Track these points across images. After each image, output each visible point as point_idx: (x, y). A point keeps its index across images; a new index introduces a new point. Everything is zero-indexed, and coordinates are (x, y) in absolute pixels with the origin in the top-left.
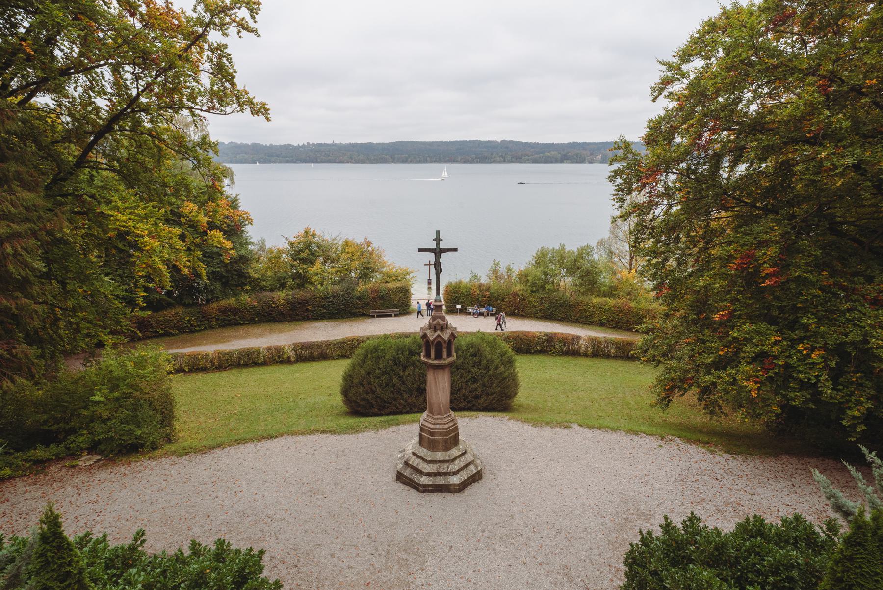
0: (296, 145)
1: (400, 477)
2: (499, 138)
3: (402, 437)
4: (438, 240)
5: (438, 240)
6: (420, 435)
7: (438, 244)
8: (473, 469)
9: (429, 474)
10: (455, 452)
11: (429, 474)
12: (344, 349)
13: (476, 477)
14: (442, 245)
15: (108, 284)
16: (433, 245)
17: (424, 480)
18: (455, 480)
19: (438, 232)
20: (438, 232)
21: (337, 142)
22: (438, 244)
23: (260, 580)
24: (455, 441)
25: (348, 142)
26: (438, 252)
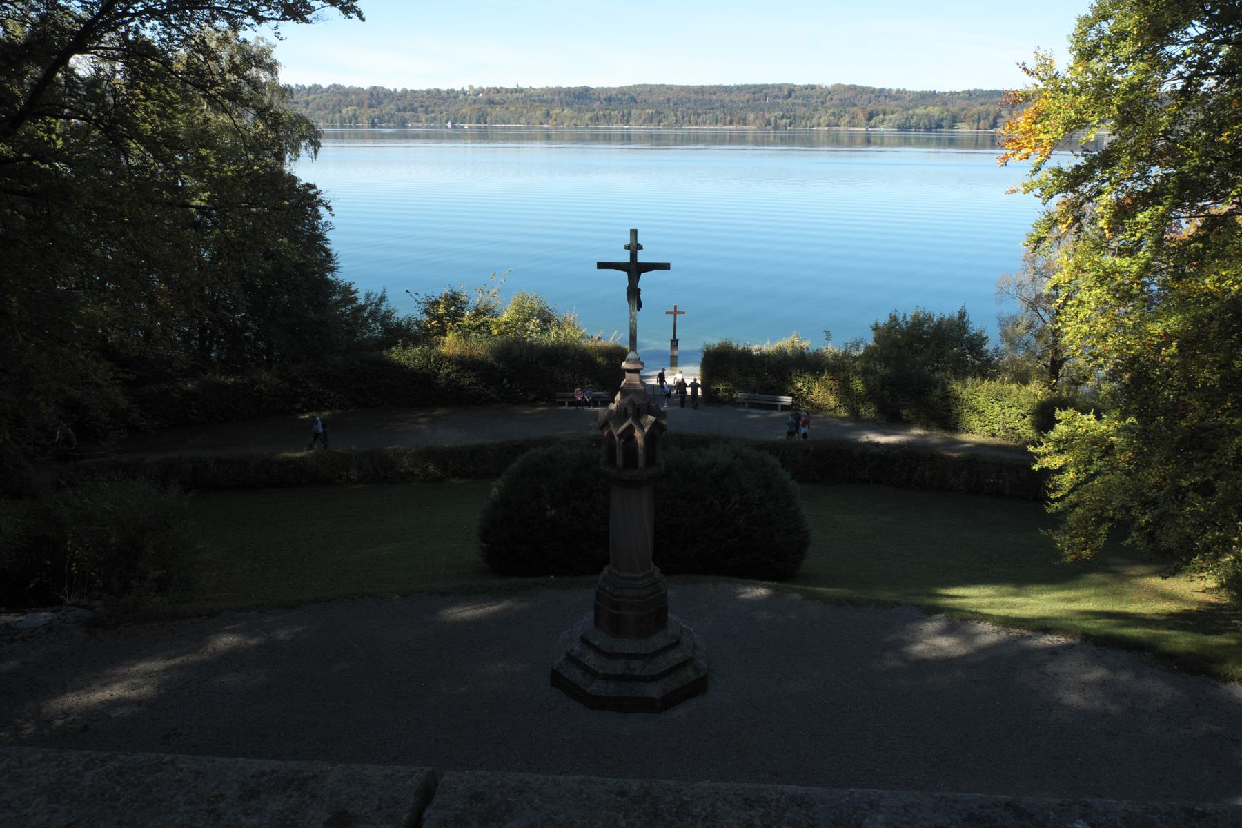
0: (347, 86)
1: (557, 679)
2: (947, 90)
3: (565, 616)
4: (634, 248)
5: (634, 248)
6: (597, 609)
7: (634, 256)
8: (689, 674)
9: (607, 678)
10: (658, 641)
11: (607, 678)
12: (468, 465)
13: (697, 688)
14: (642, 258)
15: (169, 371)
16: (625, 257)
17: (594, 688)
18: (653, 691)
19: (634, 233)
20: (634, 233)
21: (524, 85)
22: (634, 256)
23: (1003, 346)
24: (660, 620)
25: (544, 86)
26: (635, 269)
